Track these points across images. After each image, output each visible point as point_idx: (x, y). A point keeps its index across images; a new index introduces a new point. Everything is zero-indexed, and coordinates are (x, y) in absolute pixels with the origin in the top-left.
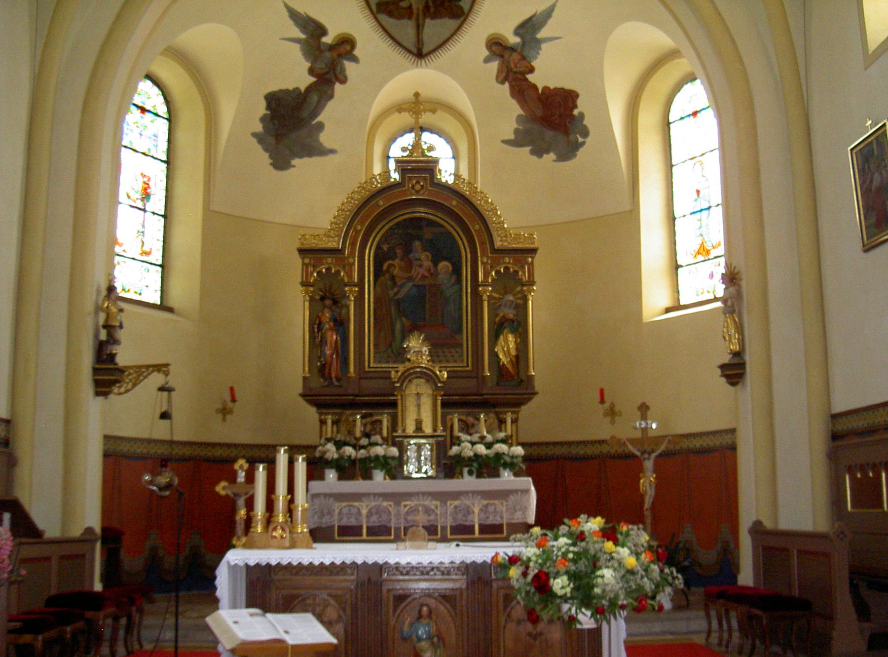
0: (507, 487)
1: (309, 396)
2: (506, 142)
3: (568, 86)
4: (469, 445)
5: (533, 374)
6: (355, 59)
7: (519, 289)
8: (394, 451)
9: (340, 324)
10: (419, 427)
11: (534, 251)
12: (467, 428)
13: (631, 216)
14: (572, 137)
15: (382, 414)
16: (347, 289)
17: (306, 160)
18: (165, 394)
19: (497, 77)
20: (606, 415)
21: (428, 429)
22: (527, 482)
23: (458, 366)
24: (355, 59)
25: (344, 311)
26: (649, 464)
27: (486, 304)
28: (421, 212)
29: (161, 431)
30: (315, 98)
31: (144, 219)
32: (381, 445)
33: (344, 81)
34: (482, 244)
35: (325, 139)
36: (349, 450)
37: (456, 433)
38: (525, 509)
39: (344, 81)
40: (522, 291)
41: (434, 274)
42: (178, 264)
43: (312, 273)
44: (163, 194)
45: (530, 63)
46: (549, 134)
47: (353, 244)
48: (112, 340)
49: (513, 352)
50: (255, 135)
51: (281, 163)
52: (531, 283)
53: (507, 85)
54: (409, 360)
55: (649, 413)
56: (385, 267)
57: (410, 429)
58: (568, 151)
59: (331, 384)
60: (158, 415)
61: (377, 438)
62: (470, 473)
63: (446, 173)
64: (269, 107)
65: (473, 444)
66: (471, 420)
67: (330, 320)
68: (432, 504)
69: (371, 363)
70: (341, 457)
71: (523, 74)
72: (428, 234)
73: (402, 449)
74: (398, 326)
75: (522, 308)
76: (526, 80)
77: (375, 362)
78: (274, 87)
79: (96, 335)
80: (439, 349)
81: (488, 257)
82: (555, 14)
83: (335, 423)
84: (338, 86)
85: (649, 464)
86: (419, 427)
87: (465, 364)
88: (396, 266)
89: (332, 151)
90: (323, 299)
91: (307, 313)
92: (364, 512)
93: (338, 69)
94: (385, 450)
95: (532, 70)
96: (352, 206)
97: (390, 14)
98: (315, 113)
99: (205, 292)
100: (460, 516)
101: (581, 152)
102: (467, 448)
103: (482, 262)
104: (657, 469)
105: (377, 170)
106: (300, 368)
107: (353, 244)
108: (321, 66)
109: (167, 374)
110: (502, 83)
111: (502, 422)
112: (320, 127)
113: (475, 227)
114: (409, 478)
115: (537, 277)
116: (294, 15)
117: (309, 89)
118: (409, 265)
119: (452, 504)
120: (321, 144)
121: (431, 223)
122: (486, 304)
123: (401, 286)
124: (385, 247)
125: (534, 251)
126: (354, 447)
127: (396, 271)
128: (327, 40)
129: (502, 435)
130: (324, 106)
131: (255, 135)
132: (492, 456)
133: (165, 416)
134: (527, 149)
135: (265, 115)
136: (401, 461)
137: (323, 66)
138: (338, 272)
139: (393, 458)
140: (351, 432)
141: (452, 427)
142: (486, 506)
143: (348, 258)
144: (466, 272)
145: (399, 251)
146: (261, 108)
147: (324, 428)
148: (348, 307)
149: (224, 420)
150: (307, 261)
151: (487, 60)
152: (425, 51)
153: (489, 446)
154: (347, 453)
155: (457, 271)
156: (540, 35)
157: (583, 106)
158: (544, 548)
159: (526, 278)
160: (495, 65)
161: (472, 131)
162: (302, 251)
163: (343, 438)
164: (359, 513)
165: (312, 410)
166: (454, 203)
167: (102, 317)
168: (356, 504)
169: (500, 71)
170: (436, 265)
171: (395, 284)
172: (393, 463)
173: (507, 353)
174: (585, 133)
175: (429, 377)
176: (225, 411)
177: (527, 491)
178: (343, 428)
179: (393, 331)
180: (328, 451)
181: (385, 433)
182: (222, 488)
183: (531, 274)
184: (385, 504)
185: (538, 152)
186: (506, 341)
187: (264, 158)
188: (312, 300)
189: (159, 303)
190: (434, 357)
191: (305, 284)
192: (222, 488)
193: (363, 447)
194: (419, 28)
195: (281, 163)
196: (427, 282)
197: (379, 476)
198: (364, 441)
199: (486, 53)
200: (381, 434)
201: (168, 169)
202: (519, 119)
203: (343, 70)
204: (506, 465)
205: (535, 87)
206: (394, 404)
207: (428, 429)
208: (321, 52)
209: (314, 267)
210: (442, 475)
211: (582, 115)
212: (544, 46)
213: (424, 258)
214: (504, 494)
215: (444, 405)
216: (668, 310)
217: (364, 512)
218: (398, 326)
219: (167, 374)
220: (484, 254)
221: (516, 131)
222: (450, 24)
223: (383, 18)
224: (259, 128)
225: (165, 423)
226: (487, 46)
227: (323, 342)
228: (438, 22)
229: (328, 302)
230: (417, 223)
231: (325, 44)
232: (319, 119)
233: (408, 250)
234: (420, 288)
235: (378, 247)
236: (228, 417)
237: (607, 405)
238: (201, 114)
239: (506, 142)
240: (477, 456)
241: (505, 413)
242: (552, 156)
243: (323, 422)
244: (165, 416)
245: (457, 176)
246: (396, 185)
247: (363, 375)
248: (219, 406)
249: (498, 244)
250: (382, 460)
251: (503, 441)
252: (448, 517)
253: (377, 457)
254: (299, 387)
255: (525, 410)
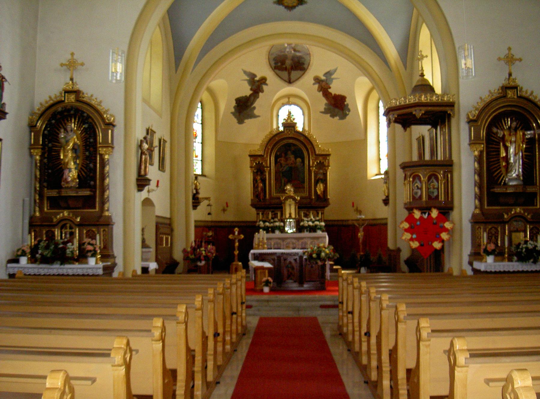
0: (319, 236)
1: (253, 205)
2: (322, 112)
3: (343, 94)
4: (306, 222)
5: (329, 197)
6: (267, 85)
7: (324, 168)
8: (282, 224)
9: (263, 181)
10: (290, 214)
11: (329, 155)
12: (306, 216)
13: (364, 142)
14: (344, 112)
15: (278, 211)
16: (265, 169)
17: (249, 120)
18: (209, 207)
19: (318, 90)
20: (355, 211)
21: (293, 216)
22: (326, 234)
23: (304, 195)
24: (267, 85)
25: (264, 177)
26: (361, 229)
27: (313, 174)
28: (291, 141)
29: (209, 218)
30: (252, 98)
31: (370, 314)
32: (278, 222)
33: (262, 91)
34: (312, 152)
35: (256, 112)
36: (267, 224)
37: (303, 218)
38: (325, 243)
39: (262, 91)
40: (325, 169)
41: (295, 163)
42: (207, 160)
43: (253, 163)
44: (201, 135)
45: (329, 86)
46: (336, 110)
47: (267, 153)
48: (197, 193)
49: (322, 190)
50: (232, 113)
51: (241, 121)
52: (328, 166)
53: (321, 93)
54: (287, 193)
55: (362, 213)
56: (278, 160)
57: (287, 216)
58: (343, 116)
59: (260, 200)
60: (207, 214)
61: (276, 219)
62: (307, 231)
63: (300, 128)
64: (236, 103)
65: (308, 221)
66: (308, 213)
67: (260, 179)
68: (294, 241)
69: (274, 194)
70: (265, 226)
71: (327, 89)
72: (293, 148)
73: (284, 223)
74: (283, 181)
75: (325, 175)
76: (328, 91)
77: (275, 193)
78: (238, 96)
79: (193, 192)
80: (298, 188)
81: (314, 157)
82: (337, 71)
83: (262, 214)
84: (260, 94)
85: (361, 229)
86: (290, 214)
87: (306, 194)
88: (282, 160)
89: (259, 116)
90: (257, 172)
91: (252, 177)
92: (273, 243)
93: (261, 88)
94: (279, 224)
95: (330, 88)
96: (267, 140)
97: (279, 70)
98: (252, 104)
99: (217, 170)
100: (303, 245)
101: (348, 117)
102: (306, 223)
103: (312, 159)
104: (364, 231)
105: (275, 127)
106: (250, 195)
107: (267, 153)
108: (254, 87)
109: (210, 201)
110: (320, 91)
111: (318, 213)
112: (254, 108)
113: (309, 147)
114: (287, 233)
115: (330, 164)
116: (245, 72)
117: (251, 95)
118: (287, 159)
119: (301, 241)
120: (255, 114)
121: (294, 145)
122: (313, 174)
123: (284, 167)
124: (278, 153)
125: (329, 155)
126: (269, 222)
127: (282, 162)
128: (257, 79)
129: (318, 218)
130: (256, 100)
131: (232, 113)
132: (314, 226)
133: (209, 214)
134: (329, 115)
135: (235, 106)
136: (284, 227)
137: (255, 87)
138: (262, 163)
139: (282, 226)
140: (268, 218)
141: (301, 216)
142: (312, 242)
143: (266, 158)
144: (306, 162)
145: (283, 155)
146: (234, 104)
147: (258, 216)
148: (266, 175)
149: (224, 213)
150: (252, 159)
151: (314, 84)
152: (292, 81)
153: (313, 222)
154: (267, 225)
155: (303, 162)
156: (333, 77)
157: (348, 101)
158: (315, 252)
159: (327, 165)
160: (317, 86)
161: (309, 104)
162: (251, 156)
163: (265, 220)
164: (271, 244)
165: (254, 210)
166: (302, 138)
167: (194, 186)
168: (270, 241)
169: (319, 87)
170: (296, 159)
171: (281, 167)
172: (282, 228)
173: (320, 190)
174: (349, 110)
175: (294, 199)
176: (224, 210)
177: (325, 237)
178: (265, 216)
179: (281, 182)
180: (260, 224)
181: (279, 218)
182: (231, 237)
183: (329, 163)
184: (279, 241)
185: (333, 116)
186: (320, 186)
187: (235, 120)
188: (254, 173)
189: (201, 174)
190: (295, 192)
191: (251, 167)
192: (231, 237)
193: (271, 223)
194: (289, 74)
195: (241, 121)
196: (293, 166)
197: (277, 232)
198: (272, 221)
199: (313, 82)
200: (277, 218)
201: (202, 126)
202: (326, 104)
203: (262, 88)
204: (318, 229)
205: (331, 94)
206: (282, 208)
207: (293, 216)
208: (255, 82)
209: (254, 161)
210: (298, 231)
211: (348, 105)
212: (334, 81)
213: (292, 157)
214: (318, 238)
215: (299, 208)
216: (377, 175)
217: (273, 243)
218: (283, 181)
219: (210, 201)
220: (312, 156)
221: (325, 109)
222: (299, 72)
223: (277, 71)
224: (233, 110)
225: (210, 216)
226: (314, 80)
227: (257, 187)
228: (296, 72)
229: (259, 173)
230: (289, 146)
231: (256, 80)
232: (254, 105)
233: (286, 154)
234: (291, 168)
235: (276, 154)
236: (225, 212)
237: (355, 208)
238: (212, 103)
239: (322, 112)
240: (309, 226)
241: (319, 211)
242: (338, 118)
243: (258, 214)
244: (209, 214)
245: (303, 129)
246: (282, 132)
247: (271, 198)
248: (222, 208)
249: (317, 152)
250: (278, 227)
251: (318, 220)
252: (176, 151)
253: (276, 226)
254: (250, 202)
255: (326, 210)
